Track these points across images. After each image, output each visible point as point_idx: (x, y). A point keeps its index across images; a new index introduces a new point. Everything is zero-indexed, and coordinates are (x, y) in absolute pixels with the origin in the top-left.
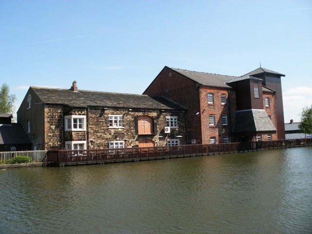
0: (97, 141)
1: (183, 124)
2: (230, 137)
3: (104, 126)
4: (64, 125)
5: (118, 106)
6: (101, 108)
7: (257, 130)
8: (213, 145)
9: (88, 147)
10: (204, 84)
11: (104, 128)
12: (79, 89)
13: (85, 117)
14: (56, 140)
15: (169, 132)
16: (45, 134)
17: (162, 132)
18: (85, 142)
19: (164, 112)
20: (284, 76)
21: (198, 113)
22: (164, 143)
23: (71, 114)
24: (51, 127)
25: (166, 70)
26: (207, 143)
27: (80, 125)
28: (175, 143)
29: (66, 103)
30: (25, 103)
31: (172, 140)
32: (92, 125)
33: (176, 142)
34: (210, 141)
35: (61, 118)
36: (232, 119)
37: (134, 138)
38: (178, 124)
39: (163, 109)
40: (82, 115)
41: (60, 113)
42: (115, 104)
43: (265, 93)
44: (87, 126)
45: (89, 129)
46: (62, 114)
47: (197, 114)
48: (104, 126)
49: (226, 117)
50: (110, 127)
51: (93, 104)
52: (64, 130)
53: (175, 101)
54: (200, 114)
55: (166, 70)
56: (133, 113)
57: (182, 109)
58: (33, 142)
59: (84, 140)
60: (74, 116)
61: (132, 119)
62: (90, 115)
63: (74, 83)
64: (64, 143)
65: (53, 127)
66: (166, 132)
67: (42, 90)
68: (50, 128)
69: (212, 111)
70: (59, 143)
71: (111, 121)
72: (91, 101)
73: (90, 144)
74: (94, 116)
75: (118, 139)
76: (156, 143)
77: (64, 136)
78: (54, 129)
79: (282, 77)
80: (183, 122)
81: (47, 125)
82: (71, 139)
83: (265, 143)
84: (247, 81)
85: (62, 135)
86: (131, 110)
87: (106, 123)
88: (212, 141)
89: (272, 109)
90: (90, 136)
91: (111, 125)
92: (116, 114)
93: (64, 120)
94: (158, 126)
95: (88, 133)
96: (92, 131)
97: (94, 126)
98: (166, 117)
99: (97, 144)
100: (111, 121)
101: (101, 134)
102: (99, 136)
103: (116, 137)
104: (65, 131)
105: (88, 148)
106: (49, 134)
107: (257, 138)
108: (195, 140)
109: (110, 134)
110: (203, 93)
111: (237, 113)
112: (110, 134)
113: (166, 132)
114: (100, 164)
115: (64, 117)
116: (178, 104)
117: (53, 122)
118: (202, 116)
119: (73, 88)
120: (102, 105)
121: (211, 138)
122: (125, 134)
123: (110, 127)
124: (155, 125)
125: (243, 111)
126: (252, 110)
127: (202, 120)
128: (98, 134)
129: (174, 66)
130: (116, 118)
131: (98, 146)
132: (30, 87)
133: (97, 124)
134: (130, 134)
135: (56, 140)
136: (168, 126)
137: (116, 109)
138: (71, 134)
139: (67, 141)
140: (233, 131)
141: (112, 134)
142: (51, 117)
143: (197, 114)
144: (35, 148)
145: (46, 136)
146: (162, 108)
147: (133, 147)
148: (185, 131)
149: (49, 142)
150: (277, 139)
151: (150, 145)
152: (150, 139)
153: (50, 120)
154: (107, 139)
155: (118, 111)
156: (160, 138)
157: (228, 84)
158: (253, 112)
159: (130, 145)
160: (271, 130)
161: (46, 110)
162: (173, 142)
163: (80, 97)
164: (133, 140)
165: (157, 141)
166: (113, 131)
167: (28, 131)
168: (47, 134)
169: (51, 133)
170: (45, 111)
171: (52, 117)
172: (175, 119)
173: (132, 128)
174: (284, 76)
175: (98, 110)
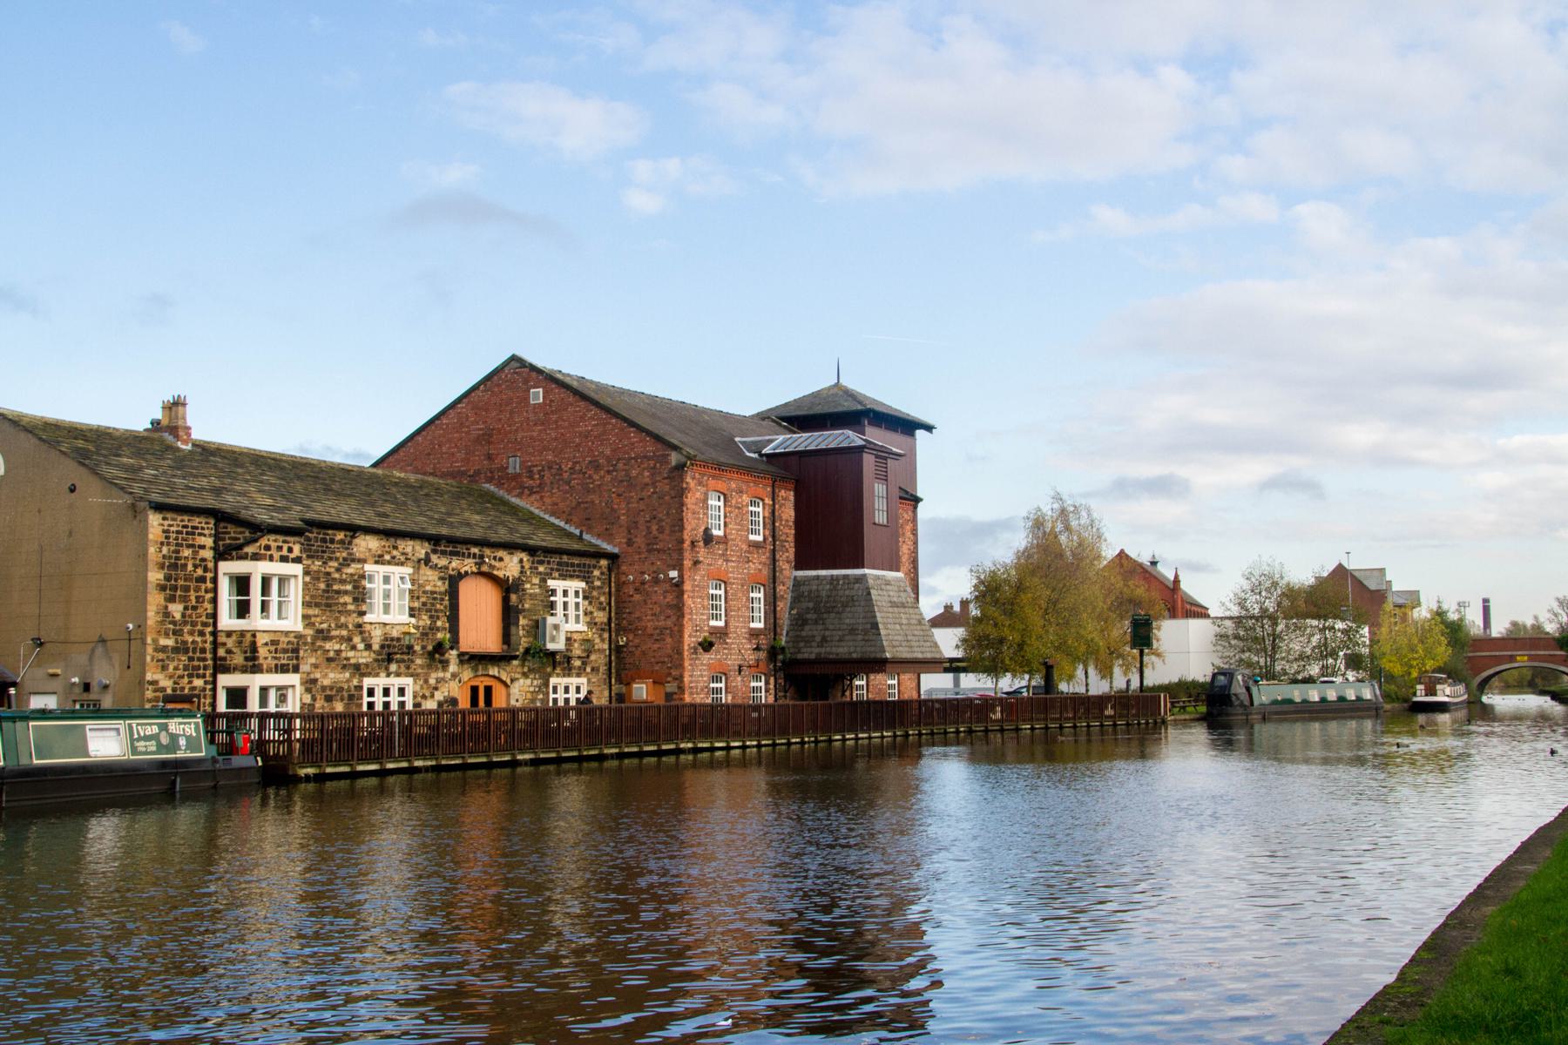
0: (326, 676)
4: (215, 601)
12: (198, 434)
26: (700, 698)
35: (206, 569)
36: (780, 605)
49: (761, 595)
52: (215, 624)
53: (553, 514)
61: (442, 587)
64: (214, 683)
75: (393, 667)
77: (215, 651)
78: (178, 616)
79: (920, 433)
92: (389, 563)
93: (215, 580)
97: (317, 611)
99: (324, 688)
101: (337, 647)
102: (332, 654)
112: (368, 647)
118: (687, 586)
122: (417, 648)
128: (328, 646)
131: (329, 699)
139: (227, 670)
148: (606, 646)
153: (168, 578)
154: (357, 667)
158: (871, 582)
159: (432, 696)
169: (167, 635)
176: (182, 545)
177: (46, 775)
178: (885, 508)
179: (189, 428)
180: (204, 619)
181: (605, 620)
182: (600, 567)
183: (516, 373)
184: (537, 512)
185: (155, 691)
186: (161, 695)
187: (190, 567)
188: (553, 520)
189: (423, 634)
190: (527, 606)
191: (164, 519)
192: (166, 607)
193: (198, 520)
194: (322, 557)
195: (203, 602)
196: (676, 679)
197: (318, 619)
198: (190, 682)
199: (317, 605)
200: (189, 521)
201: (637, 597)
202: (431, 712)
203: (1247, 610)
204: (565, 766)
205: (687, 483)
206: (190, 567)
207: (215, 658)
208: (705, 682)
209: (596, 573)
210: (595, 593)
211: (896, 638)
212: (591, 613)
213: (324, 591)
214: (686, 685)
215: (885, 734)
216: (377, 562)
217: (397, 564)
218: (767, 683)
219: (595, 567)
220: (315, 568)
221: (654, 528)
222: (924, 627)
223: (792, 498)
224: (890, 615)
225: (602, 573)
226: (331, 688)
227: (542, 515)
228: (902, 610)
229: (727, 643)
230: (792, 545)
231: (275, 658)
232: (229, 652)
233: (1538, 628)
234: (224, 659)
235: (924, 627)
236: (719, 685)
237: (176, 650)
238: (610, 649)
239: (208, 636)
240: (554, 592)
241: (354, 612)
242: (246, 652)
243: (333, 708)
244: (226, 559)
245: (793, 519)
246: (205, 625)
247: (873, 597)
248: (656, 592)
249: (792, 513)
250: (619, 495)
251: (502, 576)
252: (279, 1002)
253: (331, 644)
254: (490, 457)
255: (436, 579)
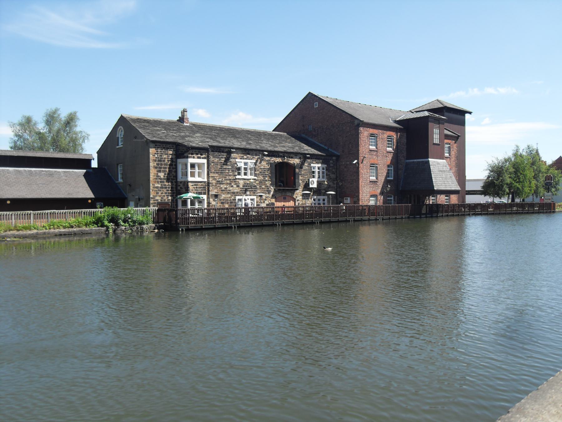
1: (333, 176)
2: (396, 197)
3: (230, 175)
5: (248, 147)
6: (227, 150)
7: (435, 189)
8: (376, 207)
9: (209, 203)
10: (366, 120)
11: (230, 178)
13: (205, 161)
14: (166, 193)
15: (315, 185)
16: (151, 185)
17: (306, 186)
18: (205, 197)
19: (308, 158)
20: (470, 113)
21: (356, 161)
22: (309, 202)
23: (187, 157)
24: (159, 174)
25: (310, 98)
27: (199, 172)
28: (321, 202)
29: (180, 141)
30: (111, 139)
31: (319, 197)
32: (214, 173)
33: (324, 200)
34: (370, 200)
37: (269, 193)
38: (327, 175)
39: (308, 154)
40: (203, 158)
41: (172, 154)
42: (244, 145)
43: (447, 136)
44: (208, 174)
45: (211, 179)
46: (174, 157)
47: (354, 162)
48: (230, 175)
49: (392, 168)
50: (238, 177)
51: (215, 144)
53: (321, 143)
54: (358, 163)
55: (310, 98)
56: (268, 158)
57: (332, 155)
58: (129, 195)
59: (204, 194)
60: (191, 161)
61: (267, 167)
62: (212, 159)
63: (184, 111)
65: (162, 175)
66: (311, 186)
67: (138, 120)
68: (158, 176)
69: (374, 159)
70: (170, 198)
71: (239, 169)
72: (211, 138)
73: (211, 200)
74: (216, 160)
75: (248, 193)
76: (298, 200)
80: (333, 173)
81: (153, 172)
82: (187, 191)
83: (442, 206)
84: (425, 119)
85: (174, 186)
86: (266, 153)
87: (232, 171)
88: (372, 202)
89: (453, 160)
90: (211, 188)
91: (239, 174)
92: (246, 159)
93: (176, 165)
94: (300, 178)
95: (208, 183)
96: (214, 182)
98: (312, 165)
100: (239, 169)
101: (225, 186)
102: (223, 189)
103: (246, 190)
104: (178, 180)
105: (208, 206)
106: (156, 185)
107: (431, 200)
108: (349, 198)
109: (238, 186)
110: (364, 133)
111: (407, 164)
113: (311, 186)
114: (231, 228)
115: (176, 162)
116: (327, 148)
117: (161, 168)
118: (361, 165)
119: (182, 120)
120: (228, 146)
121: (372, 196)
122: (258, 187)
123: (238, 177)
124: (296, 176)
125: (415, 160)
126: (430, 159)
127: (361, 171)
128: (222, 186)
129: (321, 93)
130: (246, 164)
132: (122, 116)
133: (221, 172)
134: (263, 187)
135: (166, 193)
136: (314, 177)
137: (246, 152)
138: (188, 185)
140: (400, 189)
141: (241, 186)
142: (159, 161)
143: (354, 162)
144: (132, 203)
145: (151, 188)
146: (307, 152)
147: (267, 205)
148: (335, 186)
149: (156, 196)
150: (457, 202)
151: (291, 204)
152: (290, 194)
153: (158, 164)
154: (234, 193)
155: (249, 154)
156: (303, 194)
157: (396, 122)
158: (430, 163)
159: (264, 202)
160: (453, 189)
161: (152, 150)
162: (319, 200)
163: (194, 132)
164: (268, 195)
165: (300, 198)
166: (242, 182)
167: (118, 180)
168: (154, 185)
169: (158, 182)
170: (151, 151)
171: (160, 161)
172: (319, 168)
173: (267, 179)
174: (470, 113)
175: (223, 152)
176: (163, 154)
177: (30, 229)
178: (438, 138)
179: (188, 119)
180: (172, 177)
181: (335, 177)
182: (333, 160)
183: (311, 98)
184: (316, 143)
185: (154, 201)
186: (156, 202)
187: (166, 161)
188: (321, 145)
189: (260, 182)
190: (302, 173)
191: (156, 145)
192: (158, 174)
193: (169, 146)
194: (219, 157)
195: (172, 172)
196: (357, 196)
197: (218, 178)
198: (167, 198)
199: (217, 173)
200: (165, 146)
201: (345, 169)
202: (262, 208)
203: (57, 137)
204: (371, 222)
205: (361, 130)
206: (166, 161)
207: (177, 190)
208: (368, 197)
209: (331, 162)
210: (331, 169)
211: (440, 182)
212: (329, 175)
213: (220, 168)
214: (360, 199)
215: (519, 209)
216: (241, 159)
217: (249, 159)
218: (394, 198)
219: (331, 160)
220: (216, 161)
221: (350, 146)
222: (452, 179)
223: (405, 135)
224: (438, 175)
225: (333, 162)
226: (223, 200)
227: (318, 143)
228: (444, 173)
229: (377, 185)
230: (405, 151)
231: (196, 190)
232: (181, 188)
233: (76, 126)
234: (180, 190)
235: (452, 179)
236: (391, 198)
237: (162, 188)
238: (337, 186)
239: (174, 183)
240: (314, 168)
241: (232, 175)
242: (186, 188)
243: (225, 206)
244: (181, 158)
245: (406, 142)
246: (173, 179)
247: (431, 168)
248: (351, 168)
249: (405, 140)
250: (340, 136)
251: (292, 163)
252: (108, 312)
253: (223, 185)
254: (303, 126)
255: (265, 164)
